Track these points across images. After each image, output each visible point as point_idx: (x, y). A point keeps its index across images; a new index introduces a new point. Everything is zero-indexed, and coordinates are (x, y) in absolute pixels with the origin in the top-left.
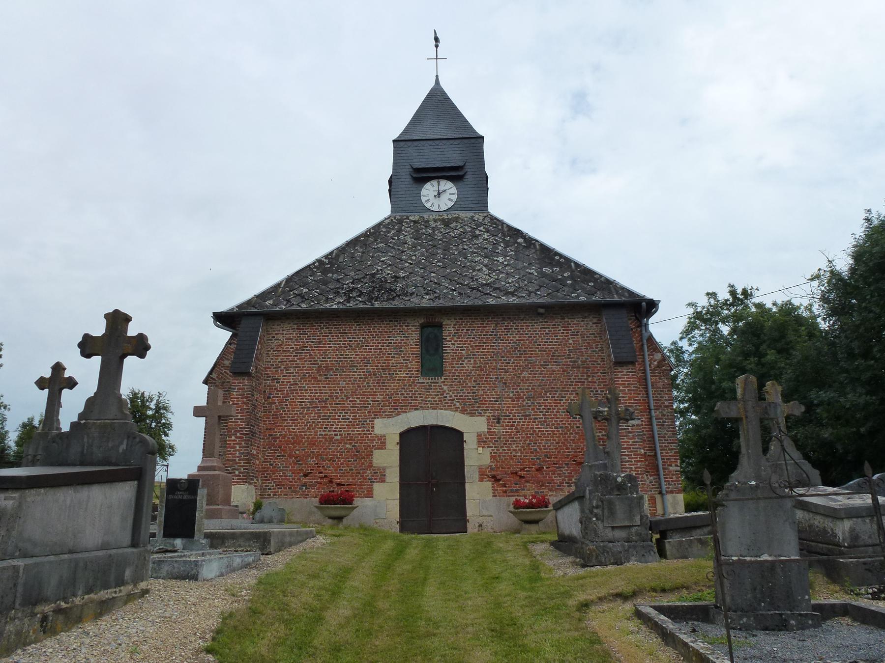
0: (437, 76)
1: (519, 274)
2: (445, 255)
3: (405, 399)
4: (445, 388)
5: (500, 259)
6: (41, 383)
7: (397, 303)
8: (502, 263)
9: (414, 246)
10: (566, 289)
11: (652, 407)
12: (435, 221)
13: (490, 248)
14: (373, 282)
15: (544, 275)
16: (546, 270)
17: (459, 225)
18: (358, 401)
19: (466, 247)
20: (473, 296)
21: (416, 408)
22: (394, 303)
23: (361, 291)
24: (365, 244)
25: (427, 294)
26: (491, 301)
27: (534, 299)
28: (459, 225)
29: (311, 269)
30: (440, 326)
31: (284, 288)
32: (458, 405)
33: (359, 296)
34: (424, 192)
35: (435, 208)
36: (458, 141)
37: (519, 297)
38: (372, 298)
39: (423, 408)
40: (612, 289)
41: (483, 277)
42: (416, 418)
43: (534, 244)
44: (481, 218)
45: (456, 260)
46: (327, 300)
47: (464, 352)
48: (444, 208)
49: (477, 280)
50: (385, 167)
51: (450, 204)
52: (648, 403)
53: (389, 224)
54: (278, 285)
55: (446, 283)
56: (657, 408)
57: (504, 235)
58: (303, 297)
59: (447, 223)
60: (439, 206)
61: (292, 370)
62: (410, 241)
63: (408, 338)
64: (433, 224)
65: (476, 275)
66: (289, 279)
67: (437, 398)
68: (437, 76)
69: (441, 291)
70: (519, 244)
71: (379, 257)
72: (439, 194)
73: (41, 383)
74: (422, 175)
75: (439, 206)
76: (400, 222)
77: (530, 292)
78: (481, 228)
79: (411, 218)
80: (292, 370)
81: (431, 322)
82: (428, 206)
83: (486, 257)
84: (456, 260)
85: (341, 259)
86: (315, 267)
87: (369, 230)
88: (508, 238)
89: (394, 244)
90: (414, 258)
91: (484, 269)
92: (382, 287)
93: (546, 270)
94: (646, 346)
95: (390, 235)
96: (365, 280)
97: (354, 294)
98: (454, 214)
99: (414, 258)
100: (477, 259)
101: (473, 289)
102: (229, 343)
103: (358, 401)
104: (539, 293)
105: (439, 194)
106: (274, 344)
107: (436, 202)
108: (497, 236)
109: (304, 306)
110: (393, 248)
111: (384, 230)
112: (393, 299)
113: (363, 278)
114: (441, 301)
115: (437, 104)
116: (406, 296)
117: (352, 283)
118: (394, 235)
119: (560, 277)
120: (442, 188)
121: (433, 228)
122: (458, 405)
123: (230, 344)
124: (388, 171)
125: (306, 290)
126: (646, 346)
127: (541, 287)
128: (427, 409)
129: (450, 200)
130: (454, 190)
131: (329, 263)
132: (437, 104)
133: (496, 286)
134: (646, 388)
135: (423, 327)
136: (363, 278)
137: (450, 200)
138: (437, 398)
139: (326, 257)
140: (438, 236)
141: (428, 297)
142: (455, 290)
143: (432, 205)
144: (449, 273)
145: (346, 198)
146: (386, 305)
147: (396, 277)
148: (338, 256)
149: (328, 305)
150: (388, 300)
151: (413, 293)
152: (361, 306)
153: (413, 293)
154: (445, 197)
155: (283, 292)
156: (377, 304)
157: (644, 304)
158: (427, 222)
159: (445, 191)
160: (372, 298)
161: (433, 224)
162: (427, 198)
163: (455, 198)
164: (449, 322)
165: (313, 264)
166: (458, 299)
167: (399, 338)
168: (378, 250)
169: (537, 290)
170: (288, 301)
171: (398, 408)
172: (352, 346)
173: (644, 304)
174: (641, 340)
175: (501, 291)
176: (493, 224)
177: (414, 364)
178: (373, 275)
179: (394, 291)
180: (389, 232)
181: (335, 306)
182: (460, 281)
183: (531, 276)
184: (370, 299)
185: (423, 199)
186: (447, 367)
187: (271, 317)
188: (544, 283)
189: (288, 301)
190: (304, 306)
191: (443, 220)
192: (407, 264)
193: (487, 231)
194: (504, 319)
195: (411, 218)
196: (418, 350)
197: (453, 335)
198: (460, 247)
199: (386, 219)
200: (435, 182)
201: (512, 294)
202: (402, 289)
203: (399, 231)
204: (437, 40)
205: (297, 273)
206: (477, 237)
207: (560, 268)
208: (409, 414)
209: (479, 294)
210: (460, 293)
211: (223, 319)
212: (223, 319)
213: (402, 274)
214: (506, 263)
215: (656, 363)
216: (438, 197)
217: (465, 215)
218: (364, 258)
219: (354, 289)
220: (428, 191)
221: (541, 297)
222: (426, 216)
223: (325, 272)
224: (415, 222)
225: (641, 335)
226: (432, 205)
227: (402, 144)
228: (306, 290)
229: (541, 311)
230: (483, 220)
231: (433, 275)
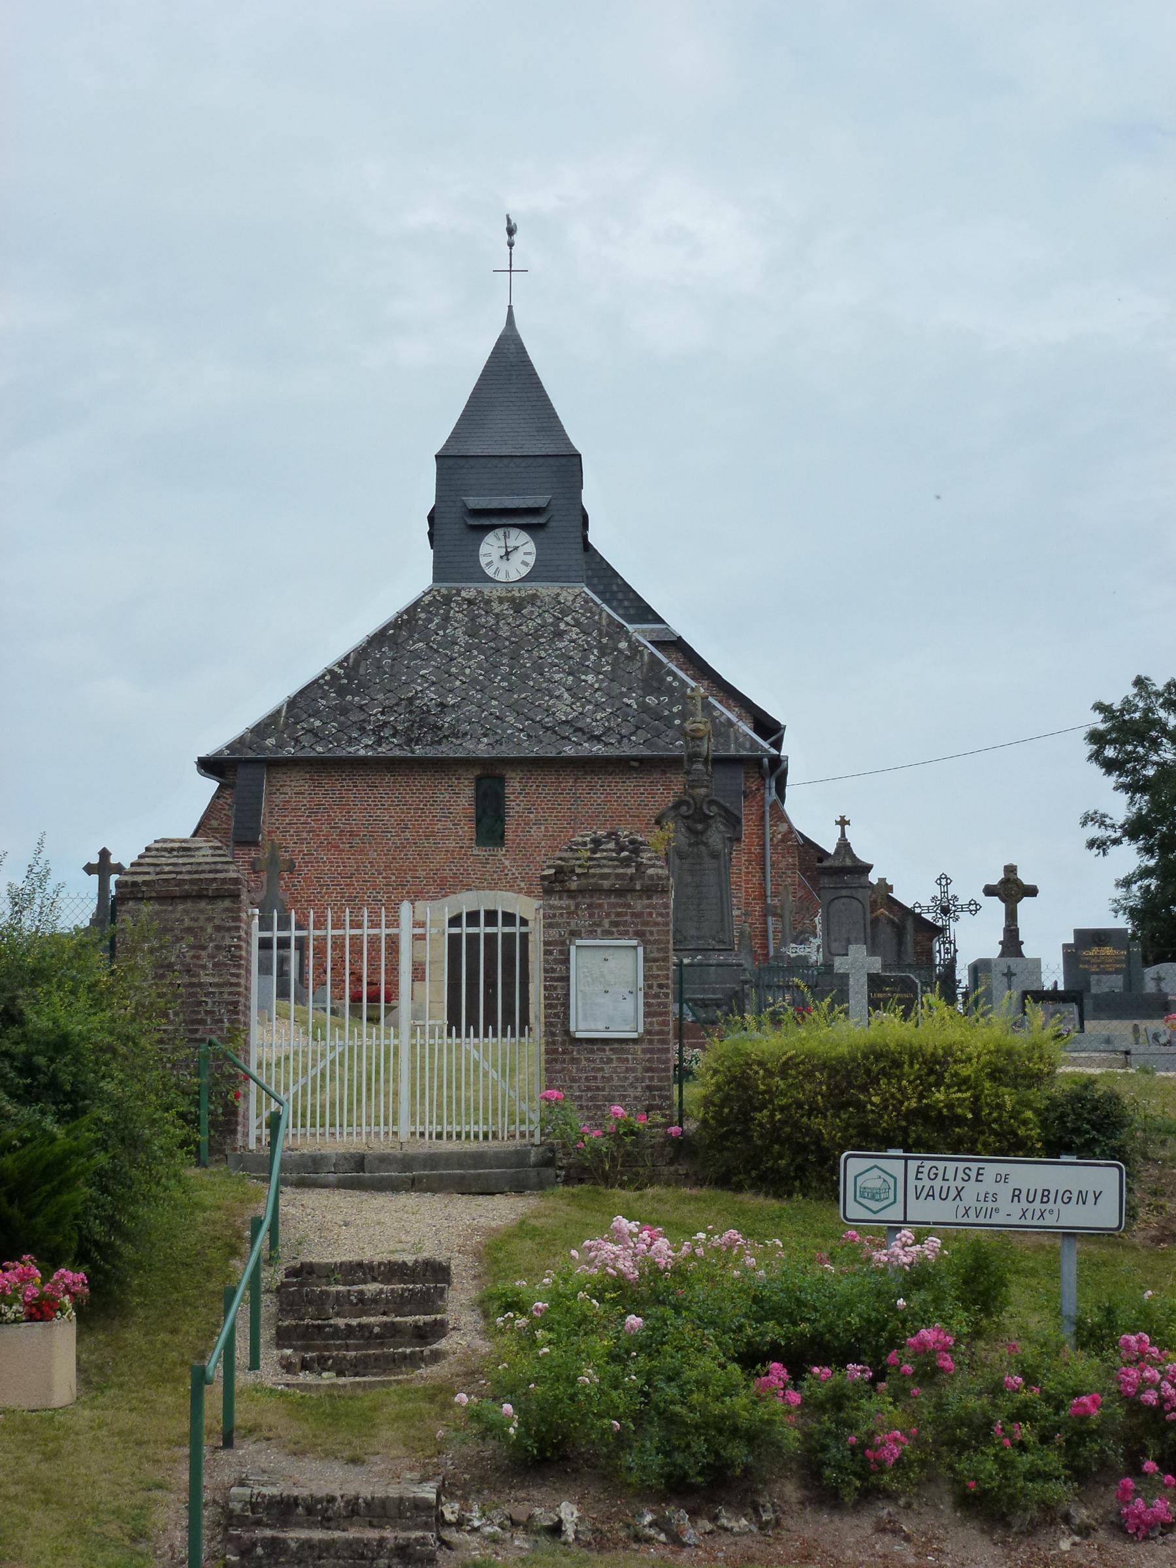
0: (510, 307)
1: (613, 705)
2: (512, 668)
3: (455, 876)
4: (507, 863)
5: (590, 678)
6: (89, 869)
7: (445, 750)
8: (592, 685)
9: (469, 648)
10: (671, 733)
11: (769, 893)
12: (501, 600)
13: (578, 657)
14: (411, 712)
15: (644, 708)
16: (651, 700)
17: (536, 611)
18: (394, 878)
19: (543, 654)
20: (546, 740)
21: (468, 888)
22: (440, 748)
23: (395, 728)
24: (394, 642)
25: (485, 735)
26: (569, 751)
27: (627, 750)
28: (536, 611)
29: (321, 687)
30: (501, 780)
31: (287, 718)
32: (522, 884)
33: (394, 736)
34: (484, 548)
35: (501, 577)
36: (541, 461)
37: (606, 744)
38: (412, 740)
39: (478, 888)
40: (732, 735)
41: (563, 711)
42: (466, 902)
43: (641, 653)
44: (571, 598)
45: (528, 677)
46: (351, 741)
47: (532, 816)
48: (514, 577)
49: (554, 713)
50: (424, 493)
51: (525, 571)
52: (765, 888)
53: (430, 604)
54: (275, 716)
55: (511, 719)
56: (775, 894)
57: (601, 635)
58: (316, 735)
59: (517, 605)
60: (507, 574)
61: (305, 835)
62: (462, 639)
63: (460, 797)
64: (496, 608)
65: (554, 705)
66: (292, 703)
67: (495, 876)
68: (510, 307)
69: (504, 731)
70: (620, 651)
71: (417, 669)
72: (507, 553)
73: (89, 869)
74: (484, 521)
75: (507, 574)
76: (447, 600)
77: (623, 737)
78: (568, 619)
79: (463, 594)
80: (305, 835)
81: (489, 781)
82: (490, 572)
83: (569, 674)
84: (528, 677)
85: (362, 671)
86: (326, 683)
87: (400, 615)
88: (604, 640)
89: (439, 644)
90: (468, 671)
91: (566, 695)
92: (423, 724)
93: (651, 700)
94: (768, 815)
95: (432, 626)
96: (400, 709)
97: (387, 732)
98: (531, 588)
99: (468, 671)
100: (557, 677)
101: (547, 729)
102: (217, 796)
103: (394, 878)
104: (633, 738)
105: (507, 553)
106: (279, 799)
107: (503, 565)
108: (589, 634)
109: (319, 749)
110: (436, 651)
111: (423, 616)
112: (439, 742)
113: (397, 704)
114: (503, 747)
115: (509, 374)
116: (457, 738)
117: (383, 713)
118: (439, 627)
119: (666, 713)
120: (512, 543)
121: (497, 615)
122: (522, 884)
123: (218, 798)
124: (429, 501)
125: (318, 723)
126: (768, 815)
127: (638, 728)
128: (483, 889)
129: (525, 563)
130: (531, 547)
131: (347, 676)
132: (509, 374)
133: (579, 725)
134: (763, 869)
135: (478, 779)
136: (397, 704)
137: (525, 563)
138: (495, 876)
139: (340, 665)
140: (504, 632)
141: (485, 740)
142: (522, 730)
143: (497, 571)
144: (517, 701)
145: (371, 566)
146: (431, 752)
147: (442, 705)
148: (357, 663)
149: (352, 750)
150: (433, 743)
151: (465, 734)
152: (397, 753)
153: (465, 734)
154: (516, 558)
155: (286, 724)
156: (419, 751)
157: (766, 760)
158: (488, 602)
159: (516, 548)
160: (412, 740)
161: (496, 608)
162: (488, 559)
163: (531, 560)
164: (513, 775)
165: (323, 676)
166: (526, 744)
167: (447, 796)
168: (415, 655)
169: (632, 734)
170: (297, 740)
171: (444, 887)
172: (383, 806)
173: (766, 760)
174: (763, 806)
175: (584, 733)
176: (586, 611)
177: (467, 830)
178: (411, 700)
179: (440, 729)
180: (431, 621)
181: (362, 752)
182: (531, 715)
183: (628, 709)
184: (409, 741)
185: (483, 561)
186: (509, 835)
187: (275, 765)
188: (643, 721)
189: (297, 740)
190: (319, 749)
191: (512, 600)
192: (458, 683)
193: (577, 624)
194: (586, 773)
195: (463, 594)
196: (472, 811)
197: (518, 794)
198: (535, 653)
199: (426, 594)
200: (500, 532)
201: (598, 739)
202: (451, 726)
203: (446, 619)
204: (511, 231)
205: (302, 692)
206: (559, 634)
207: (670, 697)
208: (459, 896)
209: (554, 737)
210: (529, 736)
211: (208, 766)
212: (208, 766)
213: (450, 700)
214: (596, 686)
215: (779, 836)
216: (508, 557)
217: (546, 590)
218: (396, 669)
219: (385, 724)
220: (490, 548)
221: (637, 744)
222: (486, 589)
223: (342, 692)
224: (470, 602)
225: (763, 799)
226: (497, 571)
227: (451, 462)
228: (318, 723)
229: (635, 764)
230: (574, 601)
231: (494, 703)
